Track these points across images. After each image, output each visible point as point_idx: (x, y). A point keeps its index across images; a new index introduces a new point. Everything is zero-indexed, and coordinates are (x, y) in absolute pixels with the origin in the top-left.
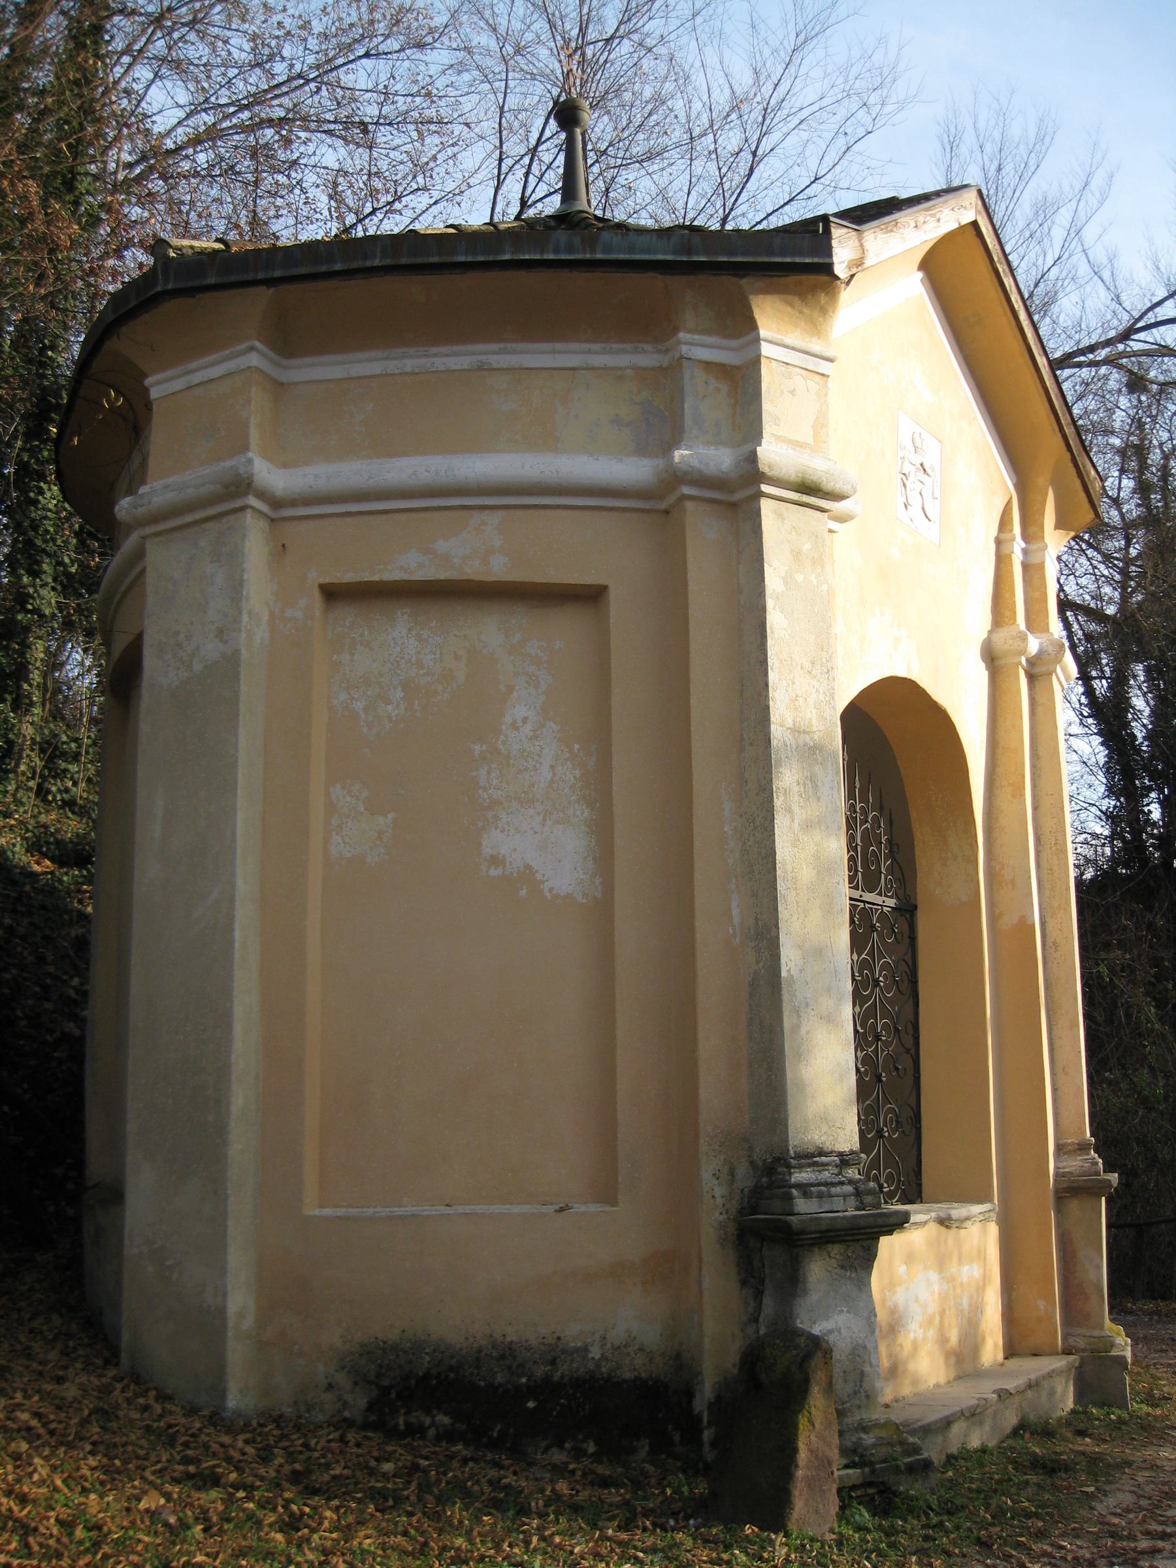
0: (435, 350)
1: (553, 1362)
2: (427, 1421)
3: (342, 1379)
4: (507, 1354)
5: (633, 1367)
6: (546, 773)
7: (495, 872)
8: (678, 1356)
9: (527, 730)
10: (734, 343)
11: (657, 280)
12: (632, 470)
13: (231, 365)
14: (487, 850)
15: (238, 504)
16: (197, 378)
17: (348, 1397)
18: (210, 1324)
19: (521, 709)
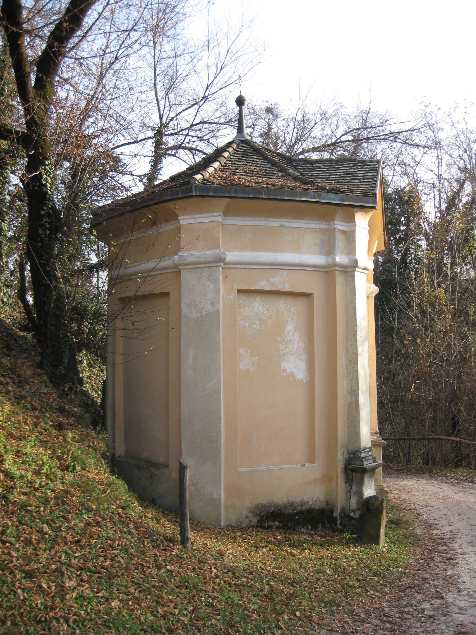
0: (269, 219)
1: (302, 506)
2: (273, 524)
3: (251, 515)
4: (292, 505)
5: (318, 506)
6: (296, 346)
7: (284, 374)
8: (327, 502)
9: (291, 333)
10: (347, 225)
11: (334, 207)
12: (320, 260)
13: (212, 219)
14: (282, 368)
15: (218, 265)
16: (199, 220)
17: (252, 519)
18: (216, 503)
19: (290, 327)
